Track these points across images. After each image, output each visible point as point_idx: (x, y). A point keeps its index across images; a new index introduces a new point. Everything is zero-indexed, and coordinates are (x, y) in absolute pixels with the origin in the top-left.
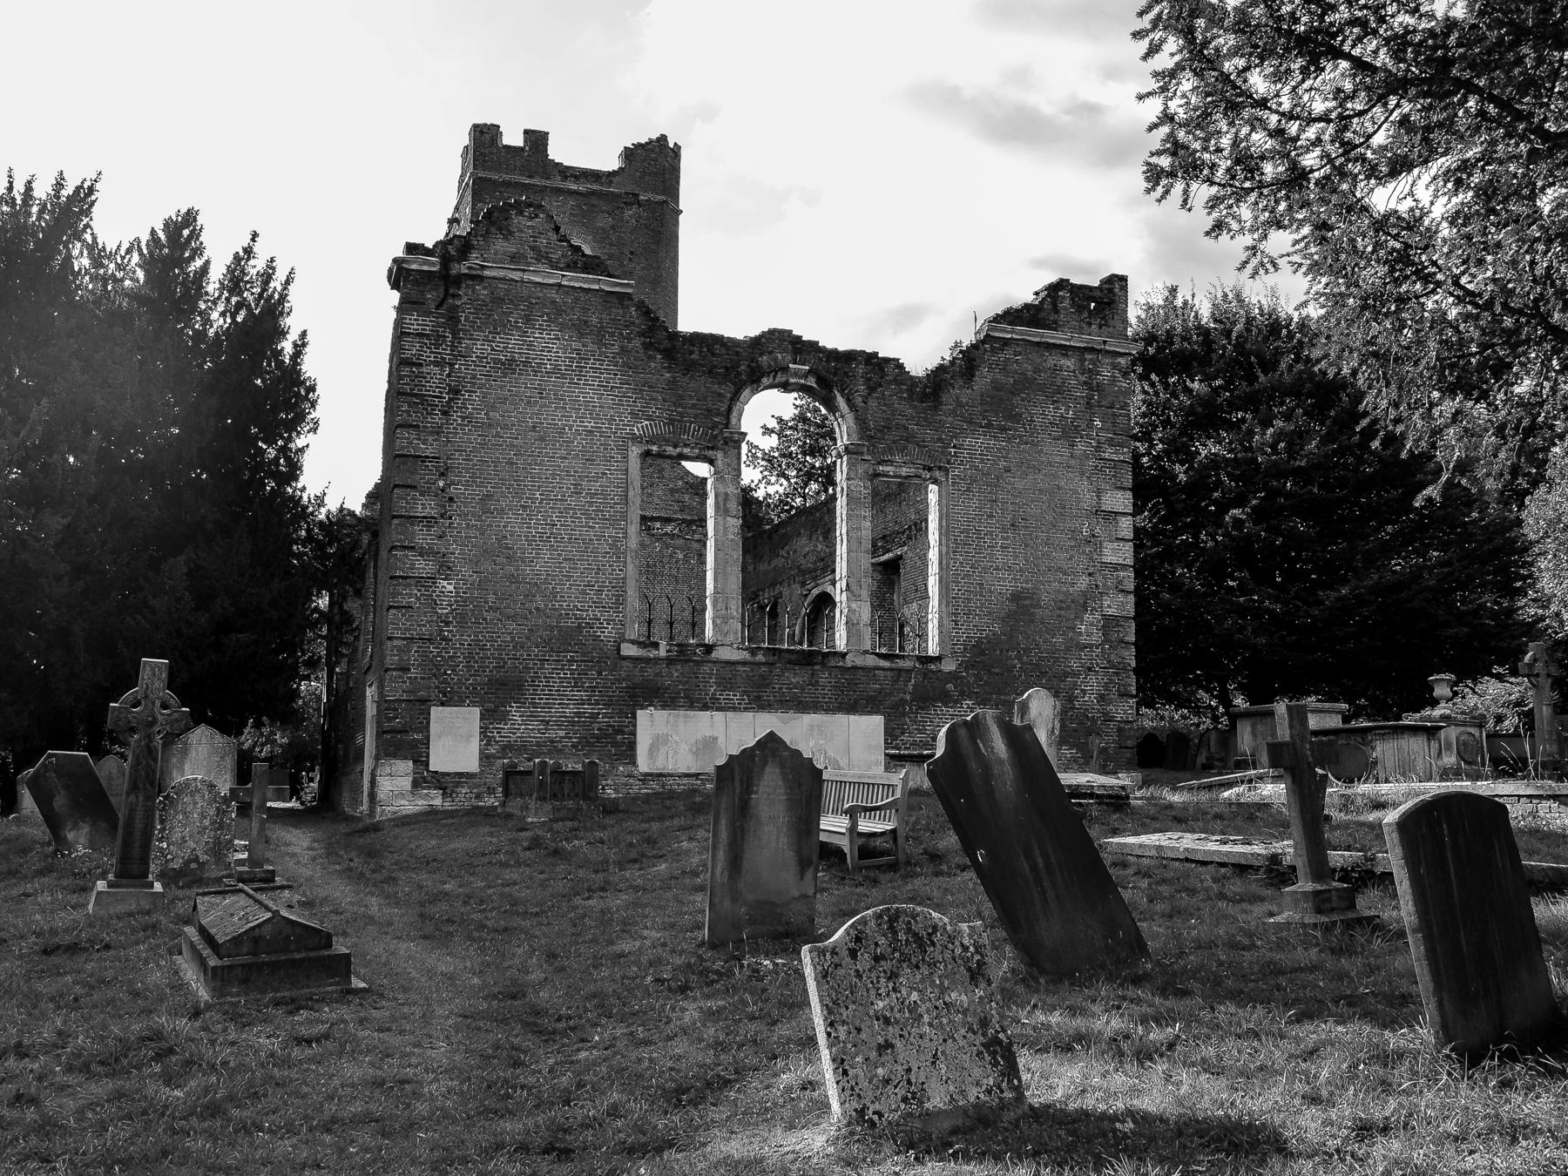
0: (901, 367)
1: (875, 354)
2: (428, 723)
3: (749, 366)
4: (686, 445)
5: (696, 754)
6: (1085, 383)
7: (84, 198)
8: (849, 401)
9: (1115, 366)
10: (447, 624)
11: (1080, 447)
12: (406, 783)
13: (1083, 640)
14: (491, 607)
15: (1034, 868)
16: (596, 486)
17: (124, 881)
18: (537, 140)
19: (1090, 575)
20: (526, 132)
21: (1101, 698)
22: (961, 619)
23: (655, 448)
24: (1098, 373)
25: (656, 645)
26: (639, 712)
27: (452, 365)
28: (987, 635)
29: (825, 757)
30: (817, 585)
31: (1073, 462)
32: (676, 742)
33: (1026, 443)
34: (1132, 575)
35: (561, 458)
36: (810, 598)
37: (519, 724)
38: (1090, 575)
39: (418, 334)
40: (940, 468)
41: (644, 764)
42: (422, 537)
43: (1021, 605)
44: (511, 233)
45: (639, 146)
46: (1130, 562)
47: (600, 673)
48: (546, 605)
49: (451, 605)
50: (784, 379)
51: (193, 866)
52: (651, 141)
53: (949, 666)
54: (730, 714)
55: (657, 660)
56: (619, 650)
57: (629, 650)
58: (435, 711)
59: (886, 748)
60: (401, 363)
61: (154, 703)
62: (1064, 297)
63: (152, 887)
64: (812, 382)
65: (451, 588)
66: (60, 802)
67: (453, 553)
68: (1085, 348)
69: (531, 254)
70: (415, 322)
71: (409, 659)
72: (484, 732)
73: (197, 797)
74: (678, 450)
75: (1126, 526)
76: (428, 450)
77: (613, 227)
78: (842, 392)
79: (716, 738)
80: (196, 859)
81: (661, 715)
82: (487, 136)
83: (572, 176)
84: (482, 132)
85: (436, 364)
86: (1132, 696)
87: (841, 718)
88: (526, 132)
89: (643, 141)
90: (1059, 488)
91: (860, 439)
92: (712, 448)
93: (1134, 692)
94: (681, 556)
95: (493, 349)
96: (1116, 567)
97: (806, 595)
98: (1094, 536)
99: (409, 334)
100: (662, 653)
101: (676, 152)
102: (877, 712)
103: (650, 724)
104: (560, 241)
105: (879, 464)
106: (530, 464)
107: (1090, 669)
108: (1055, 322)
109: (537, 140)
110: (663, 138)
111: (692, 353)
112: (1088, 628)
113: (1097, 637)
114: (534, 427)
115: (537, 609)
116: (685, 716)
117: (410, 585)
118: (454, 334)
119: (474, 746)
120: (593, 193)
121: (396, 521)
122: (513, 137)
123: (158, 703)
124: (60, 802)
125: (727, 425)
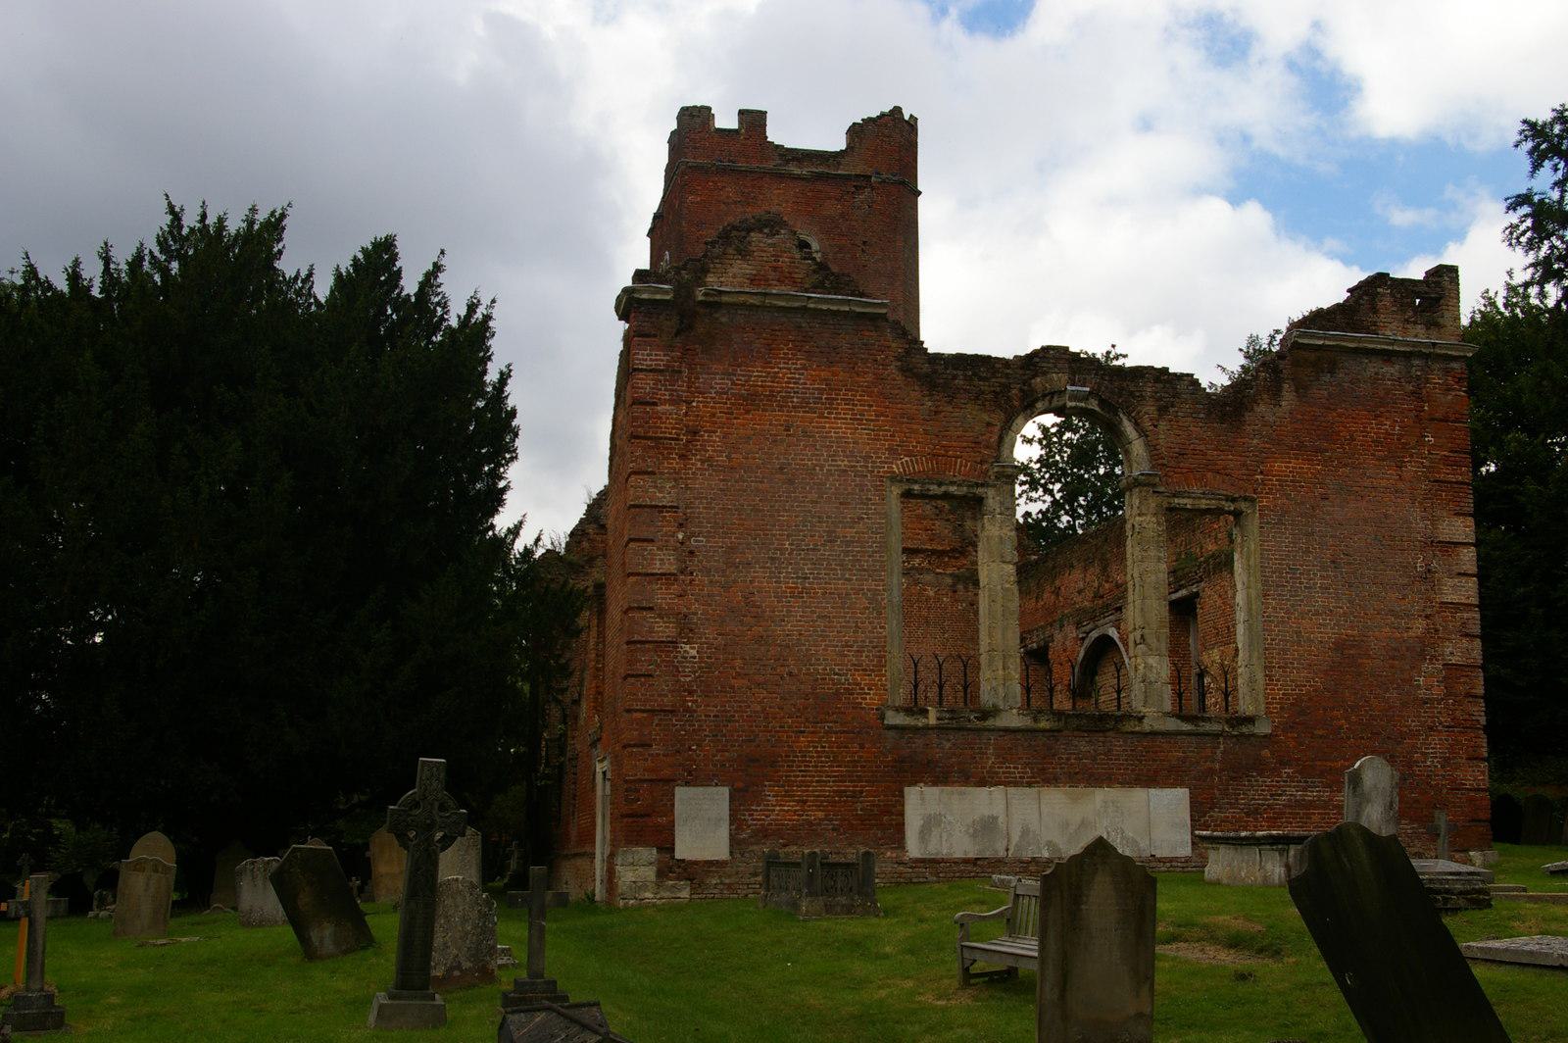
0: (1196, 383)
1: (1165, 370)
2: (673, 805)
3: (1021, 390)
4: (952, 483)
5: (974, 836)
6: (1413, 393)
7: (275, 226)
8: (1137, 425)
9: (1447, 372)
10: (691, 693)
11: (1411, 468)
12: (650, 873)
13: (1422, 693)
14: (738, 674)
15: (802, 776)
16: (851, 533)
17: (405, 992)
18: (753, 121)
19: (1427, 617)
20: (741, 113)
21: (1446, 761)
22: (1277, 673)
23: (916, 487)
24: (1427, 381)
25: (924, 712)
26: (907, 790)
27: (689, 403)
28: (1308, 692)
29: (1122, 838)
30: (1096, 627)
31: (1401, 485)
32: (950, 823)
33: (1346, 465)
34: (1477, 616)
35: (812, 502)
36: (1087, 643)
37: (775, 808)
38: (1427, 617)
39: (651, 371)
40: (1245, 499)
41: (914, 849)
42: (662, 596)
43: (1347, 654)
44: (750, 253)
45: (868, 121)
46: (1475, 600)
47: (862, 746)
48: (800, 670)
49: (694, 673)
50: (1061, 403)
51: (456, 973)
52: (883, 115)
53: (1263, 728)
54: (1011, 790)
55: (927, 728)
56: (882, 717)
57: (894, 719)
58: (681, 793)
59: (1193, 828)
60: (633, 403)
61: (432, 805)
62: (1384, 295)
63: (434, 999)
64: (1093, 405)
65: (694, 652)
66: (305, 899)
67: (695, 614)
68: (1411, 352)
69: (772, 275)
70: (645, 357)
71: (650, 733)
72: (734, 818)
73: (459, 899)
74: (943, 488)
75: (1468, 558)
76: (665, 498)
77: (842, 215)
78: (1128, 414)
79: (997, 818)
80: (459, 967)
81: (932, 792)
82: (698, 120)
83: (793, 159)
84: (692, 116)
85: (672, 402)
86: (1483, 759)
87: (1139, 795)
88: (741, 113)
89: (874, 114)
90: (1386, 516)
91: (1153, 467)
92: (982, 485)
93: (1486, 755)
94: (931, 593)
95: (733, 383)
96: (1457, 607)
97: (1083, 639)
98: (1429, 571)
99: (641, 370)
100: (932, 720)
101: (912, 125)
102: (1181, 785)
103: (919, 803)
104: (805, 259)
105: (1174, 496)
106: (778, 511)
107: (1431, 728)
108: (1375, 324)
109: (753, 121)
110: (897, 110)
111: (955, 377)
112: (1427, 680)
113: (1438, 692)
114: (781, 469)
115: (790, 674)
116: (961, 793)
117: (649, 650)
118: (690, 368)
119: (723, 833)
120: (819, 177)
121: (632, 579)
122: (726, 120)
123: (436, 804)
124: (305, 899)
125: (997, 459)
